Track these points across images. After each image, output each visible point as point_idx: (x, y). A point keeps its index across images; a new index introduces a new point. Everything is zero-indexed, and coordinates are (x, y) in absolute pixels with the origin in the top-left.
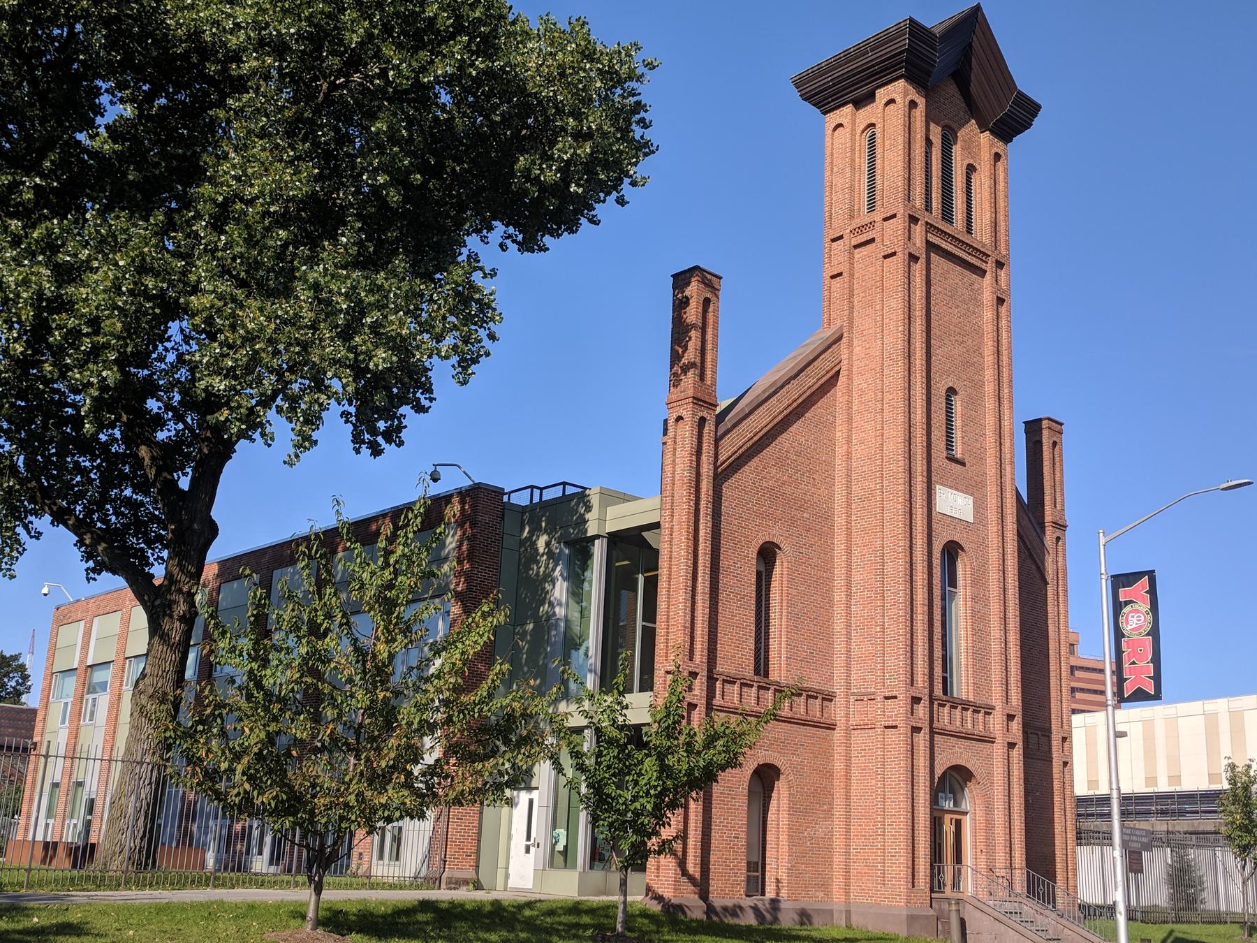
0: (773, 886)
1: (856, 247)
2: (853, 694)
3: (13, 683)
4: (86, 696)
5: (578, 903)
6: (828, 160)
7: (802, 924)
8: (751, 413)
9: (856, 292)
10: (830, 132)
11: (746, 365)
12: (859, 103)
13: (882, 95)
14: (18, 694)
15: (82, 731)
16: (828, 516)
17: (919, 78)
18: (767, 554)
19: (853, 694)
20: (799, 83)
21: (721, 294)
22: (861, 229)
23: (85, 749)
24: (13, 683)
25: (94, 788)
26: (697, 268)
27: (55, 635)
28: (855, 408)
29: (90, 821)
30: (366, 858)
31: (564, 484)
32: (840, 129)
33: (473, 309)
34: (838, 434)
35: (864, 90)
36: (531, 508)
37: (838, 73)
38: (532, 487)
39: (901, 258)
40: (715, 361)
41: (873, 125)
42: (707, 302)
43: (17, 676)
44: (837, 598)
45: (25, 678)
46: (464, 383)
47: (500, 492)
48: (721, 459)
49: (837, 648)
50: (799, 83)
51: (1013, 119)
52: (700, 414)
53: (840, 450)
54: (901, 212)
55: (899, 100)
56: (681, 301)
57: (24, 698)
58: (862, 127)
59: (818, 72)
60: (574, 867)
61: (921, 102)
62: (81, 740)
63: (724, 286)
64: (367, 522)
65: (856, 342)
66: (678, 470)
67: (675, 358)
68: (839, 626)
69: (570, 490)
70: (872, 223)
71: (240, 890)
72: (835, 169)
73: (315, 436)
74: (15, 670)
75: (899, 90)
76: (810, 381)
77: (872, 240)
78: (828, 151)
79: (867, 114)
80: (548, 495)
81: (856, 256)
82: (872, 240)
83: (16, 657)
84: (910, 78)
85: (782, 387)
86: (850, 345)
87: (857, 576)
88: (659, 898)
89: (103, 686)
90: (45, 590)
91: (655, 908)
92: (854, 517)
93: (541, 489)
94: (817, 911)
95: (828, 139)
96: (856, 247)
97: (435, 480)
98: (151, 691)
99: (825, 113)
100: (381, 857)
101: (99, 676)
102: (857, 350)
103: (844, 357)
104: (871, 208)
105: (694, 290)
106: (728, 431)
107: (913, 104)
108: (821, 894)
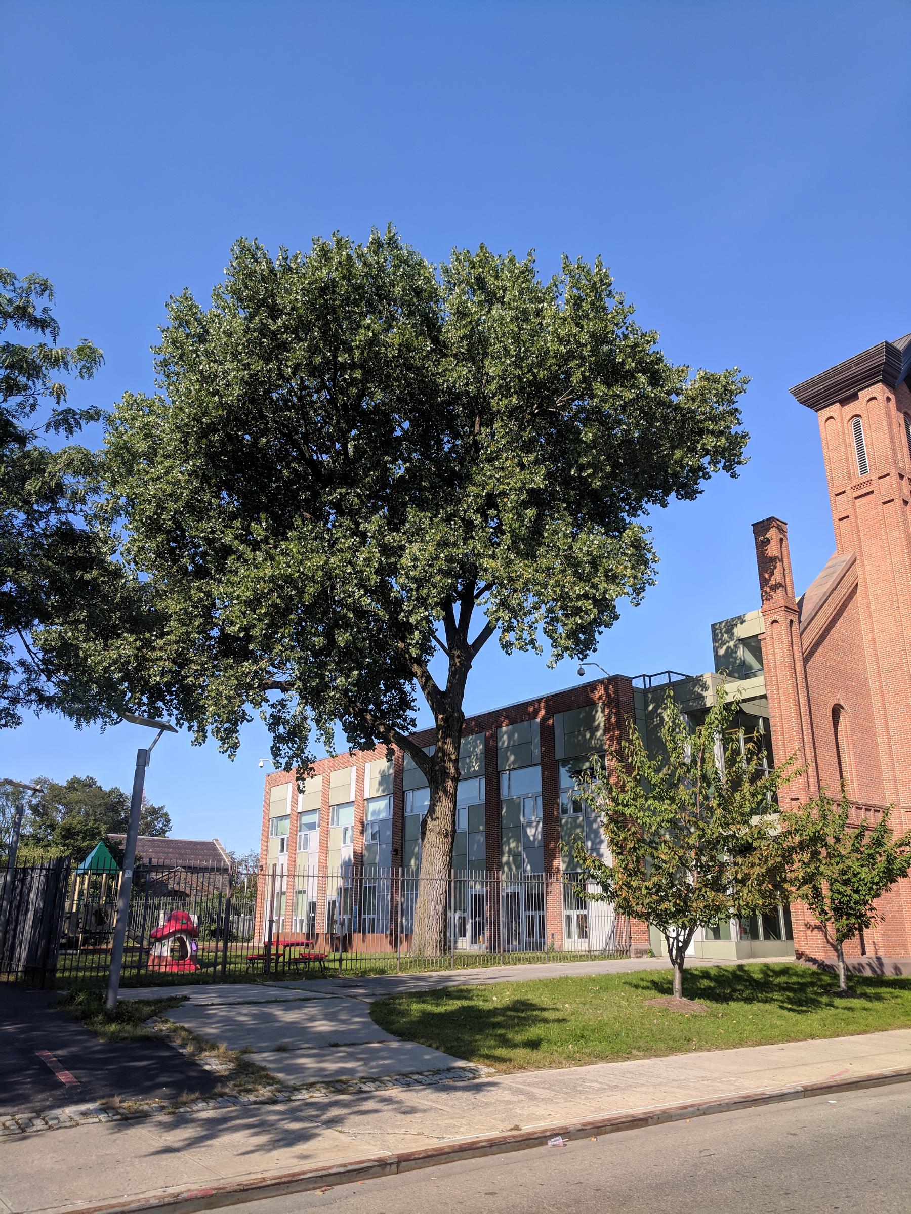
0: (872, 947)
1: (856, 498)
2: (903, 808)
3: (161, 825)
4: (299, 833)
5: (741, 967)
6: (824, 442)
7: (897, 975)
8: (815, 615)
9: (861, 528)
10: (823, 422)
11: (809, 581)
12: (844, 402)
13: (864, 395)
14: (164, 832)
15: (299, 857)
16: (866, 684)
17: (889, 383)
18: (836, 711)
19: (903, 808)
20: (796, 392)
21: (788, 534)
22: (860, 486)
23: (302, 868)
24: (161, 825)
25: (315, 894)
26: (772, 519)
27: (268, 794)
28: (873, 607)
29: (314, 918)
30: (557, 937)
31: (669, 672)
32: (831, 420)
33: (640, 554)
34: (863, 626)
35: (848, 393)
36: (645, 691)
37: (829, 383)
38: (644, 676)
39: (898, 502)
40: (791, 580)
41: (859, 416)
42: (781, 540)
43: (163, 820)
44: (880, 740)
45: (168, 821)
46: (638, 605)
47: (629, 680)
48: (804, 648)
49: (885, 775)
50: (796, 392)
51: (621, 444)
52: (790, 618)
53: (866, 638)
54: (894, 473)
55: (879, 397)
56: (762, 542)
57: (167, 834)
58: (848, 418)
59: (813, 383)
60: (728, 938)
61: (892, 397)
62: (298, 863)
63: (788, 528)
64: (524, 706)
65: (866, 563)
66: (778, 658)
67: (764, 582)
68: (884, 759)
69: (675, 678)
70: (869, 481)
71: (503, 967)
72: (830, 448)
73: (515, 650)
74: (161, 817)
75: (879, 390)
76: (843, 591)
77: (872, 492)
78: (823, 436)
79: (851, 408)
80: (656, 682)
81: (857, 504)
82: (872, 492)
83: (162, 808)
84: (885, 382)
85: (829, 596)
86: (863, 565)
87: (893, 725)
88: (814, 961)
89: (311, 826)
90: (261, 764)
91: (814, 968)
92: (884, 684)
93: (650, 677)
94: (903, 964)
95: (821, 428)
96: (856, 498)
97: (582, 675)
98: (438, 829)
99: (817, 411)
100: (569, 936)
101: (306, 819)
102: (868, 568)
103: (860, 573)
104: (864, 470)
105: (772, 533)
106: (805, 628)
107: (888, 399)
108: (903, 952)
